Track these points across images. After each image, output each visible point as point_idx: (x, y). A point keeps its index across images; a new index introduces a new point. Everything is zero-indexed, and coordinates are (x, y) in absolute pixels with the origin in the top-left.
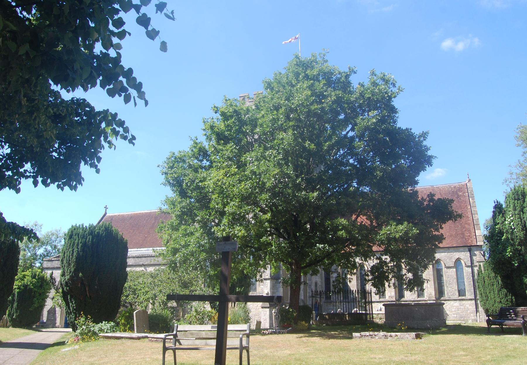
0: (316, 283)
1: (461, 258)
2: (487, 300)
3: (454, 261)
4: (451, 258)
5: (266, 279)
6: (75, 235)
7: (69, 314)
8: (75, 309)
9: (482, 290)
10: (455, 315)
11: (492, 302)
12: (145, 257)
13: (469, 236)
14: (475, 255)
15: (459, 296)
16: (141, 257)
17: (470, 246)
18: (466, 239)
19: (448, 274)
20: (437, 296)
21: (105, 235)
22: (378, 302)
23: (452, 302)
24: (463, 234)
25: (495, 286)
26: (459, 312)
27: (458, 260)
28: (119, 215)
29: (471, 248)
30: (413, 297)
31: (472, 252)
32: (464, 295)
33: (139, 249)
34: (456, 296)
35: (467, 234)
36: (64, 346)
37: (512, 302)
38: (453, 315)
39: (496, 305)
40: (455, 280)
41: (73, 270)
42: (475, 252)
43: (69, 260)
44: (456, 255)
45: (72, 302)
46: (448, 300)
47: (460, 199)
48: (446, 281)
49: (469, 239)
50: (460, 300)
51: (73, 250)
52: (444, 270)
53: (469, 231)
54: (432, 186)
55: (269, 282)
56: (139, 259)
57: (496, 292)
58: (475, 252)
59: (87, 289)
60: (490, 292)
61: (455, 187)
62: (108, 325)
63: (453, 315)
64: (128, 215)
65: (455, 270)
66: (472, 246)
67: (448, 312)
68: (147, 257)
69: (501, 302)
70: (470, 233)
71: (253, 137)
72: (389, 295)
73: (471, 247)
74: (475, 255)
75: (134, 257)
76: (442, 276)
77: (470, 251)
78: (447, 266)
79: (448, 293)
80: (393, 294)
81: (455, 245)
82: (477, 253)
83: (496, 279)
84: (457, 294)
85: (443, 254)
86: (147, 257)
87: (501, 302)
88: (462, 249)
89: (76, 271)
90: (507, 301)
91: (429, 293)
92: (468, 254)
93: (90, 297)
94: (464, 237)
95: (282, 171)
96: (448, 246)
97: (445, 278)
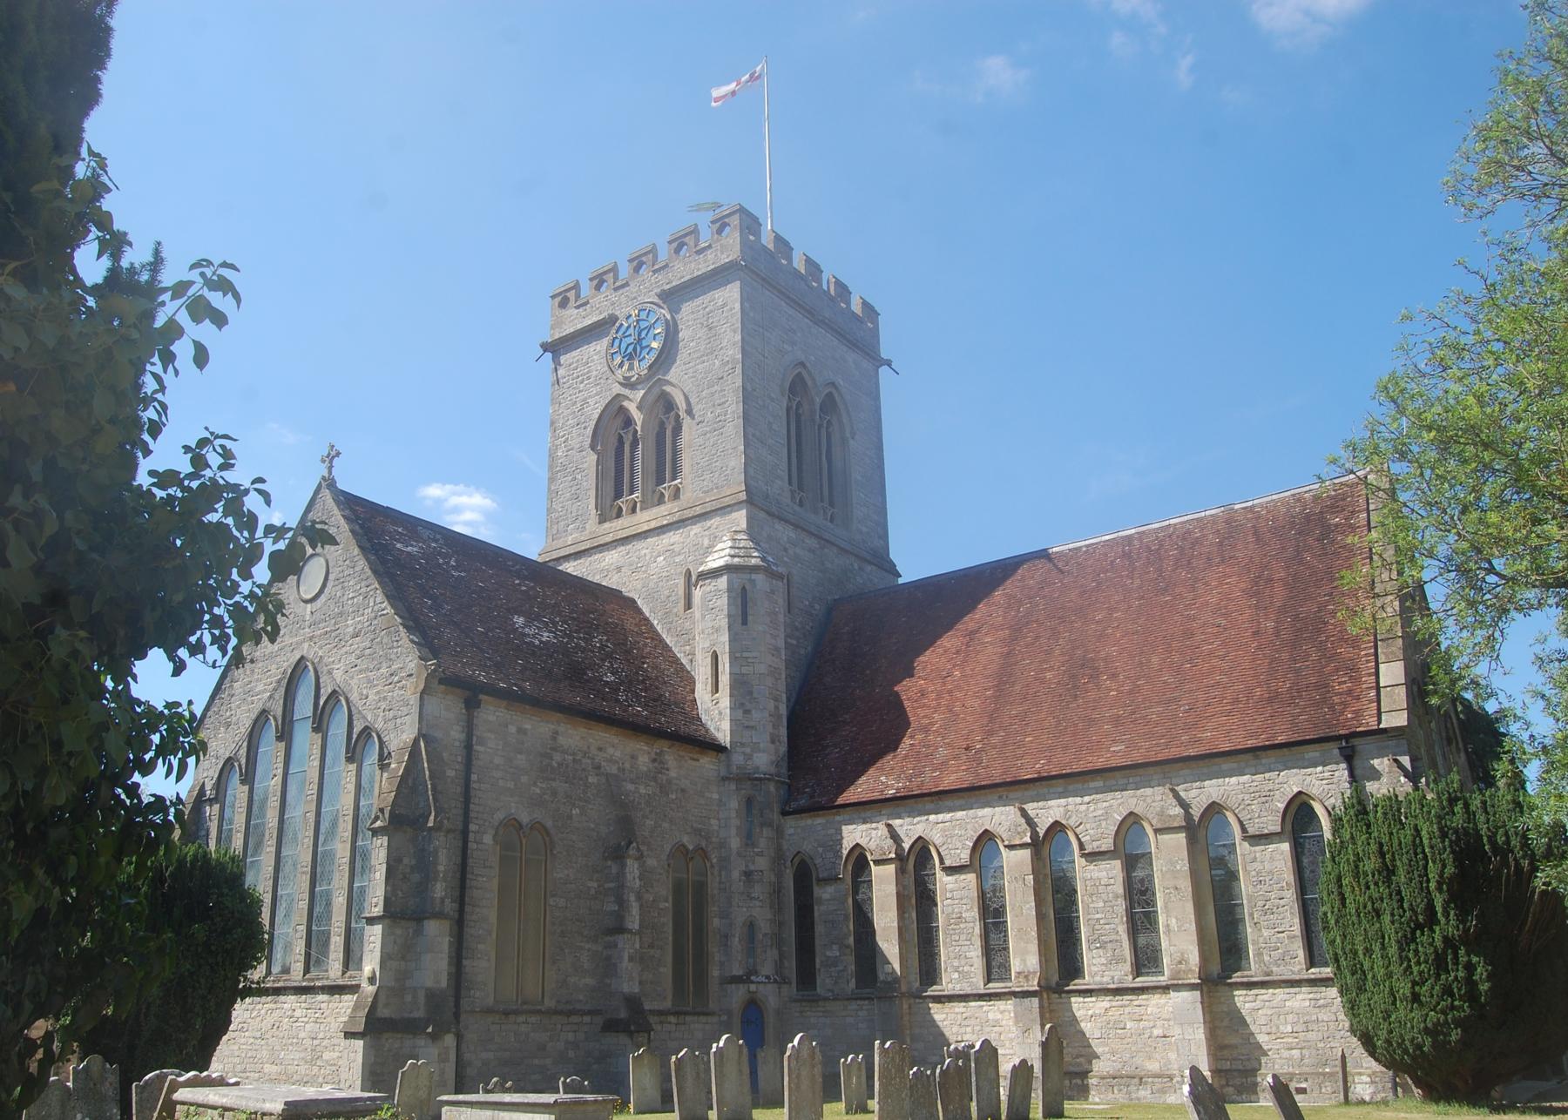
1: (1314, 791)
2: (1361, 989)
3: (1282, 806)
4: (1268, 797)
9: (1338, 940)
10: (1296, 1053)
11: (1380, 1000)
13: (1350, 692)
14: (1375, 775)
15: (989, 980)
17: (1348, 737)
20: (1215, 968)
24: (1323, 686)
25: (1387, 918)
26: (1311, 1036)
27: (1131, 823)
29: (1350, 748)
30: (1117, 975)
31: (1357, 763)
32: (1005, 977)
34: (1122, 973)
35: (1340, 685)
37: (1472, 995)
39: (1402, 1012)
40: (1290, 895)
42: (1376, 762)
44: (1292, 781)
47: (1333, 542)
48: (1250, 898)
49: (1345, 705)
50: (1313, 982)
52: (1243, 848)
53: (1352, 670)
54: (1298, 499)
57: (1393, 950)
58: (1376, 762)
60: (1368, 951)
61: (1316, 498)
63: (1286, 1054)
65: (1286, 847)
67: (1262, 1038)
69: (1416, 998)
70: (1356, 680)
73: (1356, 741)
74: (1375, 775)
77: (1349, 757)
78: (1251, 831)
79: (1259, 954)
80: (1033, 962)
81: (1281, 739)
82: (1381, 764)
83: (1388, 882)
84: (1301, 953)
85: (1234, 780)
88: (1312, 752)
90: (1447, 991)
91: (1177, 956)
92: (1342, 772)
94: (1324, 700)
96: (1251, 743)
97: (1245, 887)
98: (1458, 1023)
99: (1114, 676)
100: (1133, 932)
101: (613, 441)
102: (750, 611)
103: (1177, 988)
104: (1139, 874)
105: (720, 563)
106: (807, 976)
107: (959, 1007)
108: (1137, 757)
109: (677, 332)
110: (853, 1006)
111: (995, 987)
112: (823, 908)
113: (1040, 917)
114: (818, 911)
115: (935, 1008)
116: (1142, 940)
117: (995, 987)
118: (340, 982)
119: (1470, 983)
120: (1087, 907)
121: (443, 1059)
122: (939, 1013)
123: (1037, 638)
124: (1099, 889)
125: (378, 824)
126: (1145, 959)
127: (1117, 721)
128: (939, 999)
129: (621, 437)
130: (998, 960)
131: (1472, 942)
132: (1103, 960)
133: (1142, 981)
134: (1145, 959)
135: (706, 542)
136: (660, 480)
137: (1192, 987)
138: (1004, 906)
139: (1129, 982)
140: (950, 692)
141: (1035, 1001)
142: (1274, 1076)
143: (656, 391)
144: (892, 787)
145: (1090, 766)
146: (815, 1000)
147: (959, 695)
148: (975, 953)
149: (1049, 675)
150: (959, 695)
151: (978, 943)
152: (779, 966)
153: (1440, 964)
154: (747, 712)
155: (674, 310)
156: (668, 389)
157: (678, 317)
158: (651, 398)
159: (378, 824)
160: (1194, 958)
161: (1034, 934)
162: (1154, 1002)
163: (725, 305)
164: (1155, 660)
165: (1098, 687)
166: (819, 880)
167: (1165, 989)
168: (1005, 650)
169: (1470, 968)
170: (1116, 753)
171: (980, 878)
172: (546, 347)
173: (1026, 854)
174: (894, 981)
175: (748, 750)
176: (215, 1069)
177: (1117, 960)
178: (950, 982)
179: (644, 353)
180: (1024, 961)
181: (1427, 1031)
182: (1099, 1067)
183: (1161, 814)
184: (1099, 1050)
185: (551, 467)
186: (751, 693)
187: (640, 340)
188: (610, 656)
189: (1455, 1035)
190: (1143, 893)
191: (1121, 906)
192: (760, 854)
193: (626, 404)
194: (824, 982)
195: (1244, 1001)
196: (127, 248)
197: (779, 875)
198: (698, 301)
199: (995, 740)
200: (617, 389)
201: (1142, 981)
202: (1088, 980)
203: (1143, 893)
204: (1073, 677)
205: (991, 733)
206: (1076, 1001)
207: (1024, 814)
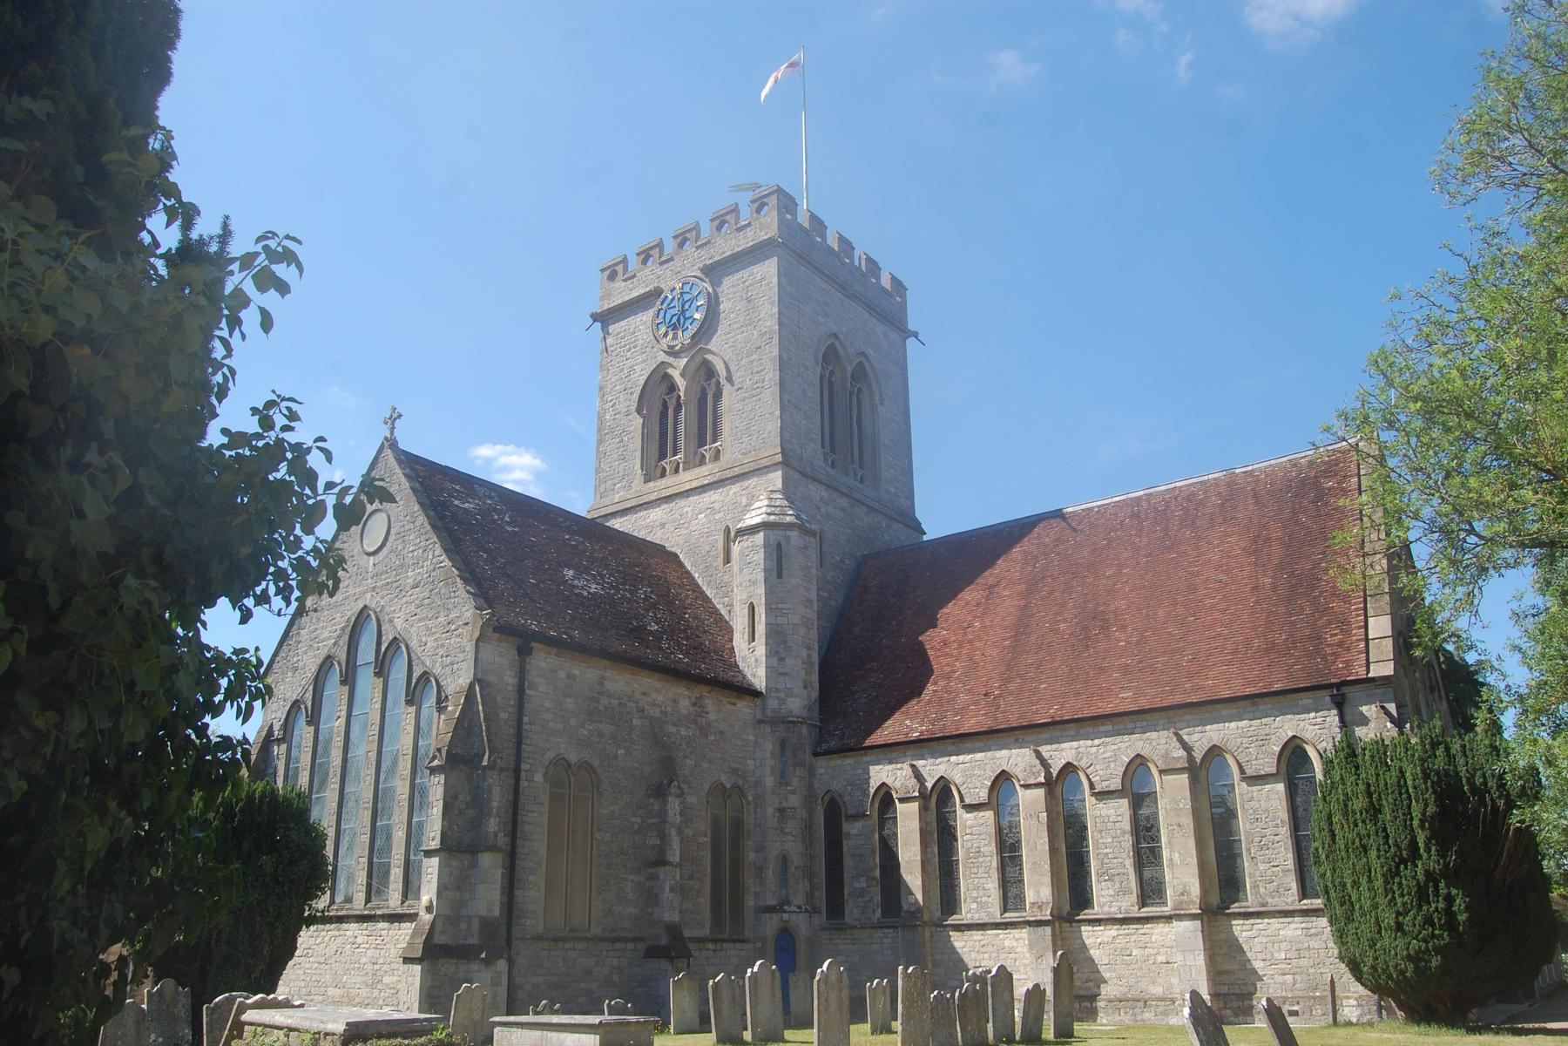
1: (1307, 736)
3: (1277, 749)
4: (1265, 739)
9: (1328, 874)
10: (1289, 978)
11: (1366, 930)
13: (1340, 644)
14: (1364, 721)
15: (1005, 909)
17: (1339, 685)
18: (1324, 658)
19: (1254, 804)
20: (1215, 900)
22: (997, 926)
23: (1274, 923)
24: (1317, 638)
25: (1373, 854)
29: (1342, 696)
30: (1124, 905)
31: (1348, 710)
34: (1128, 904)
35: (1332, 637)
36: (846, 1009)
37: (1451, 925)
38: (1279, 979)
40: (1285, 831)
42: (1364, 709)
44: (1286, 726)
46: (1259, 915)
49: (1336, 655)
53: (1344, 624)
57: (1379, 883)
58: (1364, 709)
60: (1356, 884)
61: (1311, 463)
63: (1279, 979)
65: (1281, 787)
66: (1345, 683)
67: (1257, 965)
69: (1399, 927)
70: (1347, 632)
71: (1476, 440)
73: (1346, 689)
74: (1364, 721)
77: (1340, 704)
78: (1249, 772)
79: (1255, 886)
80: (1046, 893)
81: (1277, 687)
82: (1370, 710)
83: (1375, 820)
84: (1294, 886)
85: (1233, 725)
88: (1306, 699)
90: (1429, 921)
91: (1180, 889)
92: (1333, 717)
96: (1248, 691)
98: (1438, 950)
99: (1123, 628)
100: (1140, 865)
101: (658, 407)
102: (785, 565)
103: (1179, 917)
104: (1144, 811)
105: (757, 520)
106: (835, 907)
107: (977, 935)
108: (1144, 703)
109: (718, 304)
110: (879, 933)
111: (1011, 916)
112: (851, 843)
113: (1053, 851)
114: (847, 845)
116: (1147, 874)
117: (1011, 916)
118: (399, 911)
119: (1450, 913)
121: (495, 982)
122: (959, 941)
123: (1052, 592)
124: (1107, 825)
126: (1150, 891)
127: (1125, 670)
128: (959, 928)
129: (665, 403)
130: (1013, 891)
131: (1452, 876)
132: (1110, 891)
134: (1150, 891)
135: (744, 501)
137: (1193, 917)
138: (1019, 841)
139: (1135, 912)
140: (970, 642)
141: (1048, 930)
142: (1269, 1000)
143: (698, 359)
144: (916, 730)
145: (1100, 712)
146: (844, 929)
147: (978, 644)
148: (992, 885)
149: (1062, 626)
150: (978, 644)
151: (995, 875)
152: (810, 896)
153: (1422, 896)
154: (781, 659)
155: (716, 284)
156: (709, 357)
157: (719, 290)
158: (694, 366)
159: (436, 763)
160: (1195, 890)
161: (1047, 867)
162: (1158, 931)
163: (762, 279)
164: (1161, 613)
165: (1108, 637)
166: (847, 817)
167: (1168, 919)
168: (1022, 603)
169: (1449, 899)
170: (1125, 700)
171: (997, 815)
172: (595, 317)
173: (1041, 792)
174: (917, 912)
175: (782, 695)
177: (1125, 892)
178: (969, 911)
180: (1038, 892)
182: (1107, 991)
183: (1166, 756)
184: (1107, 975)
185: (599, 430)
186: (785, 642)
187: (683, 311)
188: (654, 607)
189: (1435, 962)
190: (1149, 829)
191: (1128, 841)
192: (793, 792)
194: (852, 911)
195: (1240, 929)
197: (811, 812)
199: (1011, 686)
200: (662, 357)
202: (1096, 911)
203: (1149, 829)
204: (1085, 628)
205: (1008, 680)
206: (1086, 930)
207: (1039, 755)
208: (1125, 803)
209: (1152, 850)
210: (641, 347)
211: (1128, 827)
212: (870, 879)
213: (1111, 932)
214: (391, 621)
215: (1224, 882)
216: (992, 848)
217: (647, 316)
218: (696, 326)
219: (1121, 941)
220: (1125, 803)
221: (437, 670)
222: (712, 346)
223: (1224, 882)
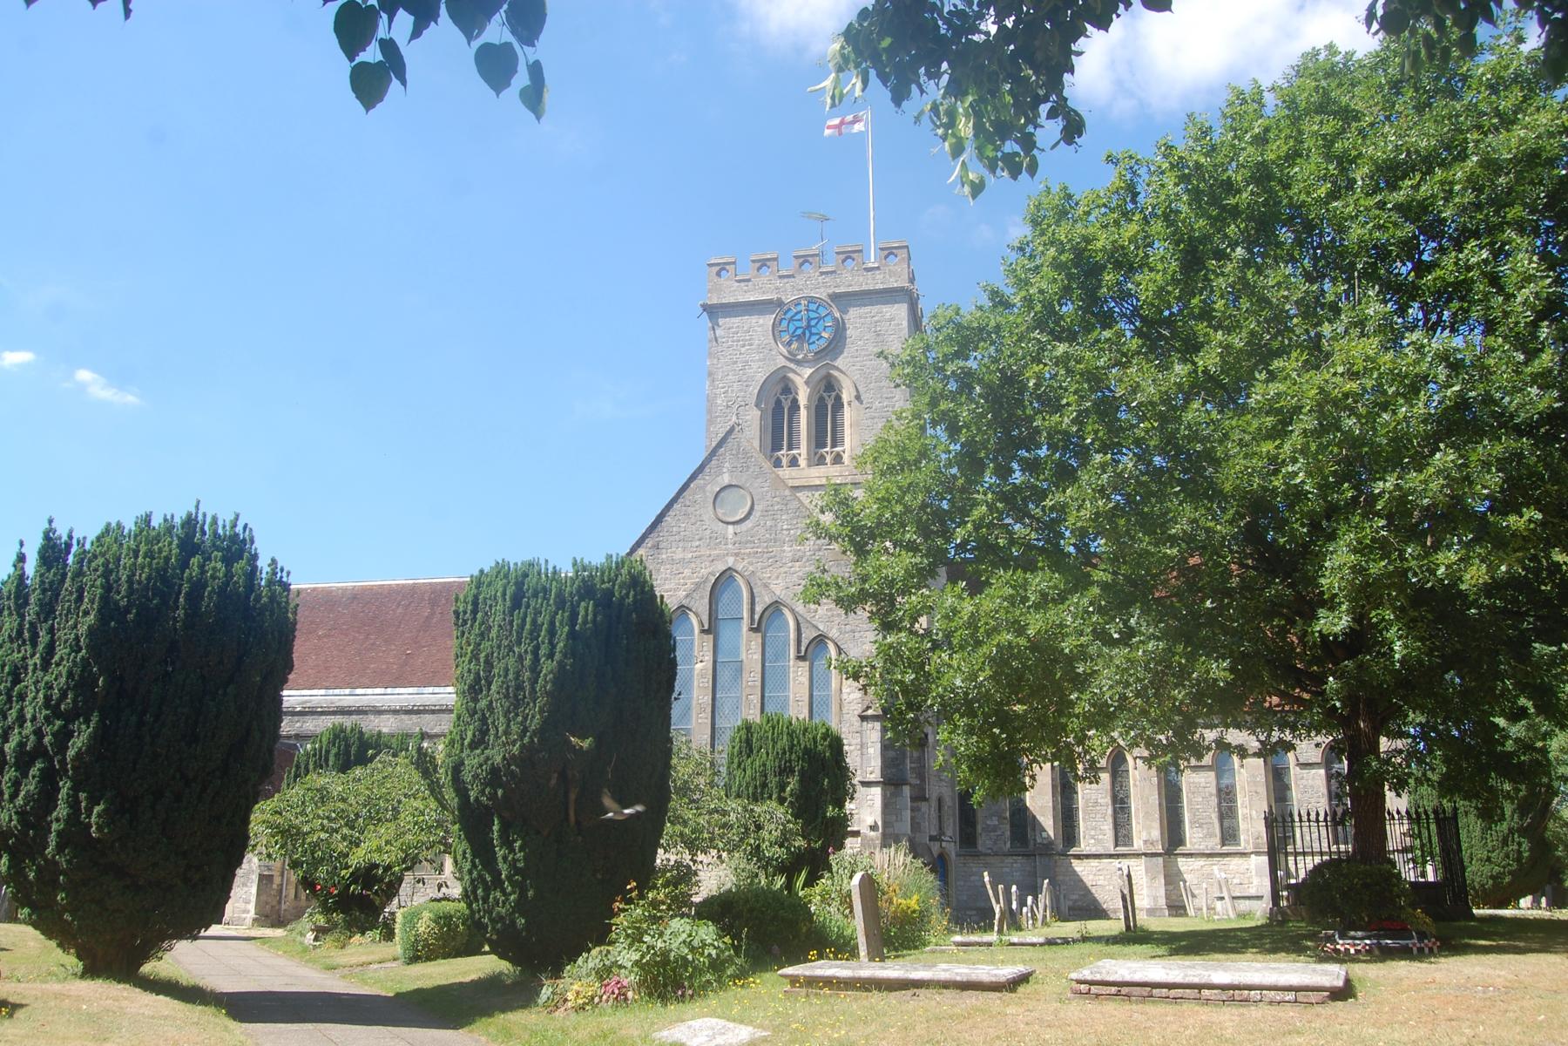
0: (940, 800)
5: (866, 784)
6: (535, 595)
7: (487, 890)
8: (518, 871)
12: (433, 712)
15: (1116, 845)
16: (418, 712)
21: (635, 601)
22: (1111, 856)
28: (314, 589)
30: (1210, 844)
33: (389, 690)
34: (1214, 843)
37: (1519, 859)
41: (535, 723)
43: (519, 687)
45: (507, 843)
51: (537, 648)
52: (1294, 771)
55: (876, 792)
56: (414, 717)
59: (572, 796)
62: (1360, 945)
64: (345, 590)
68: (440, 711)
69: (1489, 859)
72: (1144, 836)
75: (395, 712)
76: (1287, 788)
80: (1156, 834)
86: (440, 711)
87: (1489, 859)
89: (553, 726)
93: (578, 823)
95: (1339, 429)
98: (1510, 873)
100: (1221, 818)
101: (772, 405)
107: (1094, 863)
109: (845, 329)
110: (1010, 860)
111: (1121, 850)
113: (1054, 808)
115: (1075, 862)
116: (1226, 824)
117: (1121, 850)
119: (1519, 852)
120: (1190, 802)
122: (1079, 867)
125: (870, 712)
126: (1229, 835)
128: (1078, 857)
129: (778, 402)
130: (1123, 832)
131: (1523, 831)
132: (1193, 837)
133: (1226, 849)
134: (1121, 831)
136: (776, 446)
139: (1218, 849)
141: (1160, 860)
143: (823, 372)
146: (977, 855)
148: (1108, 827)
151: (1110, 820)
153: (1505, 842)
155: (844, 311)
156: (835, 373)
157: (846, 317)
158: (818, 377)
159: (870, 712)
162: (1235, 862)
163: (891, 320)
169: (1520, 844)
171: (1218, 777)
172: (705, 308)
174: (1049, 845)
176: (226, 917)
177: (1211, 835)
178: (1085, 845)
179: (814, 338)
181: (1492, 877)
185: (709, 412)
187: (809, 327)
189: (1507, 879)
191: (1214, 800)
193: (791, 375)
194: (984, 842)
196: (395, 83)
198: (868, 309)
200: (781, 362)
201: (1226, 849)
202: (1189, 846)
206: (1181, 860)
208: (1212, 774)
209: (1230, 808)
210: (754, 351)
211: (1214, 791)
212: (1001, 818)
213: (1201, 862)
214: (766, 586)
215: (1174, 836)
216: (1108, 800)
217: (768, 320)
218: (823, 343)
219: (1207, 870)
220: (1212, 774)
221: (834, 633)
222: (839, 363)
223: (1174, 836)
